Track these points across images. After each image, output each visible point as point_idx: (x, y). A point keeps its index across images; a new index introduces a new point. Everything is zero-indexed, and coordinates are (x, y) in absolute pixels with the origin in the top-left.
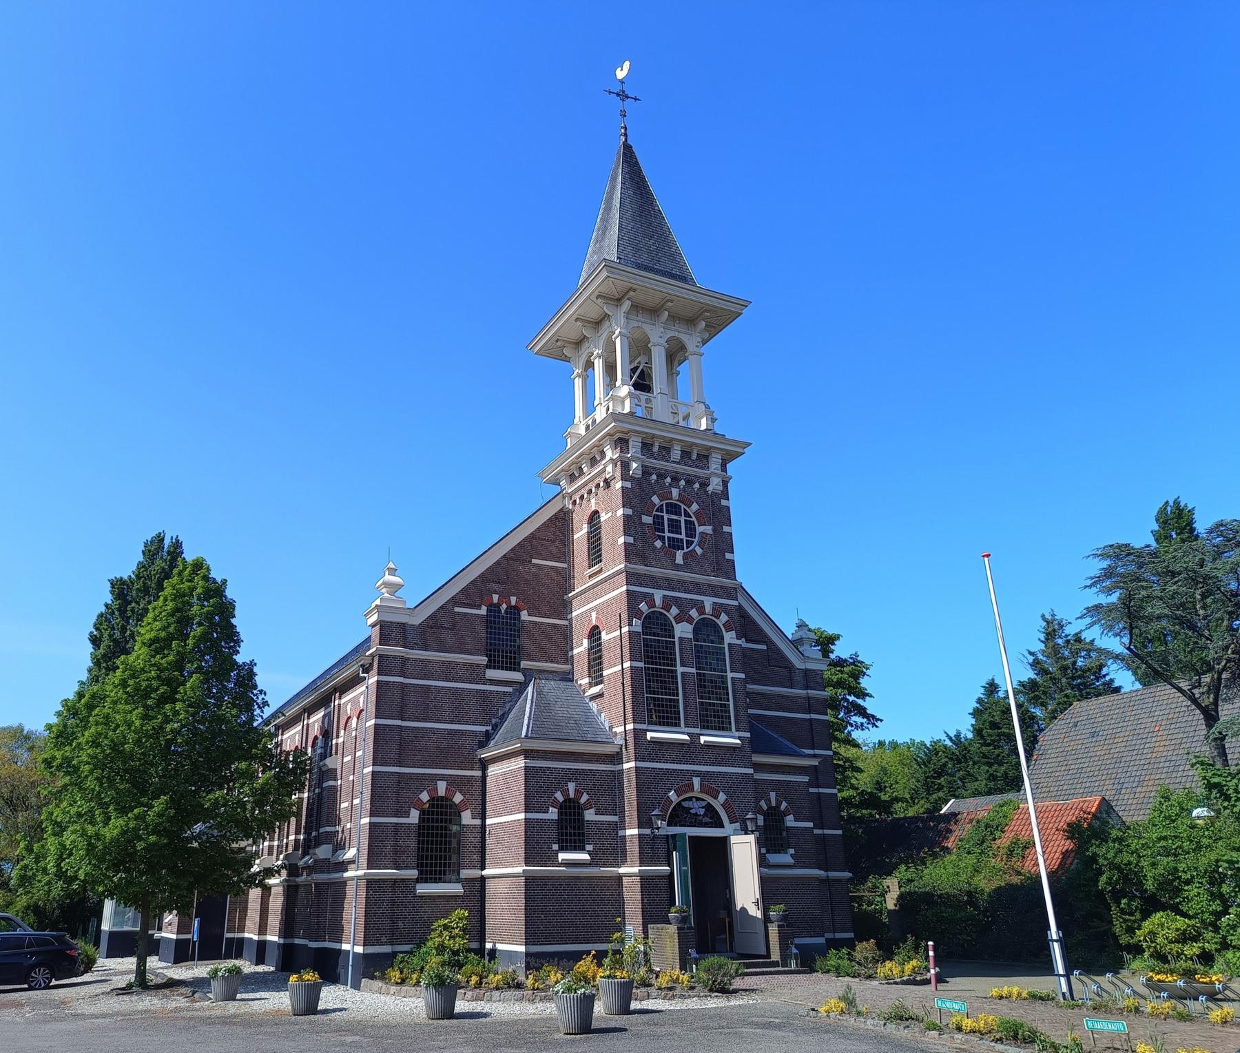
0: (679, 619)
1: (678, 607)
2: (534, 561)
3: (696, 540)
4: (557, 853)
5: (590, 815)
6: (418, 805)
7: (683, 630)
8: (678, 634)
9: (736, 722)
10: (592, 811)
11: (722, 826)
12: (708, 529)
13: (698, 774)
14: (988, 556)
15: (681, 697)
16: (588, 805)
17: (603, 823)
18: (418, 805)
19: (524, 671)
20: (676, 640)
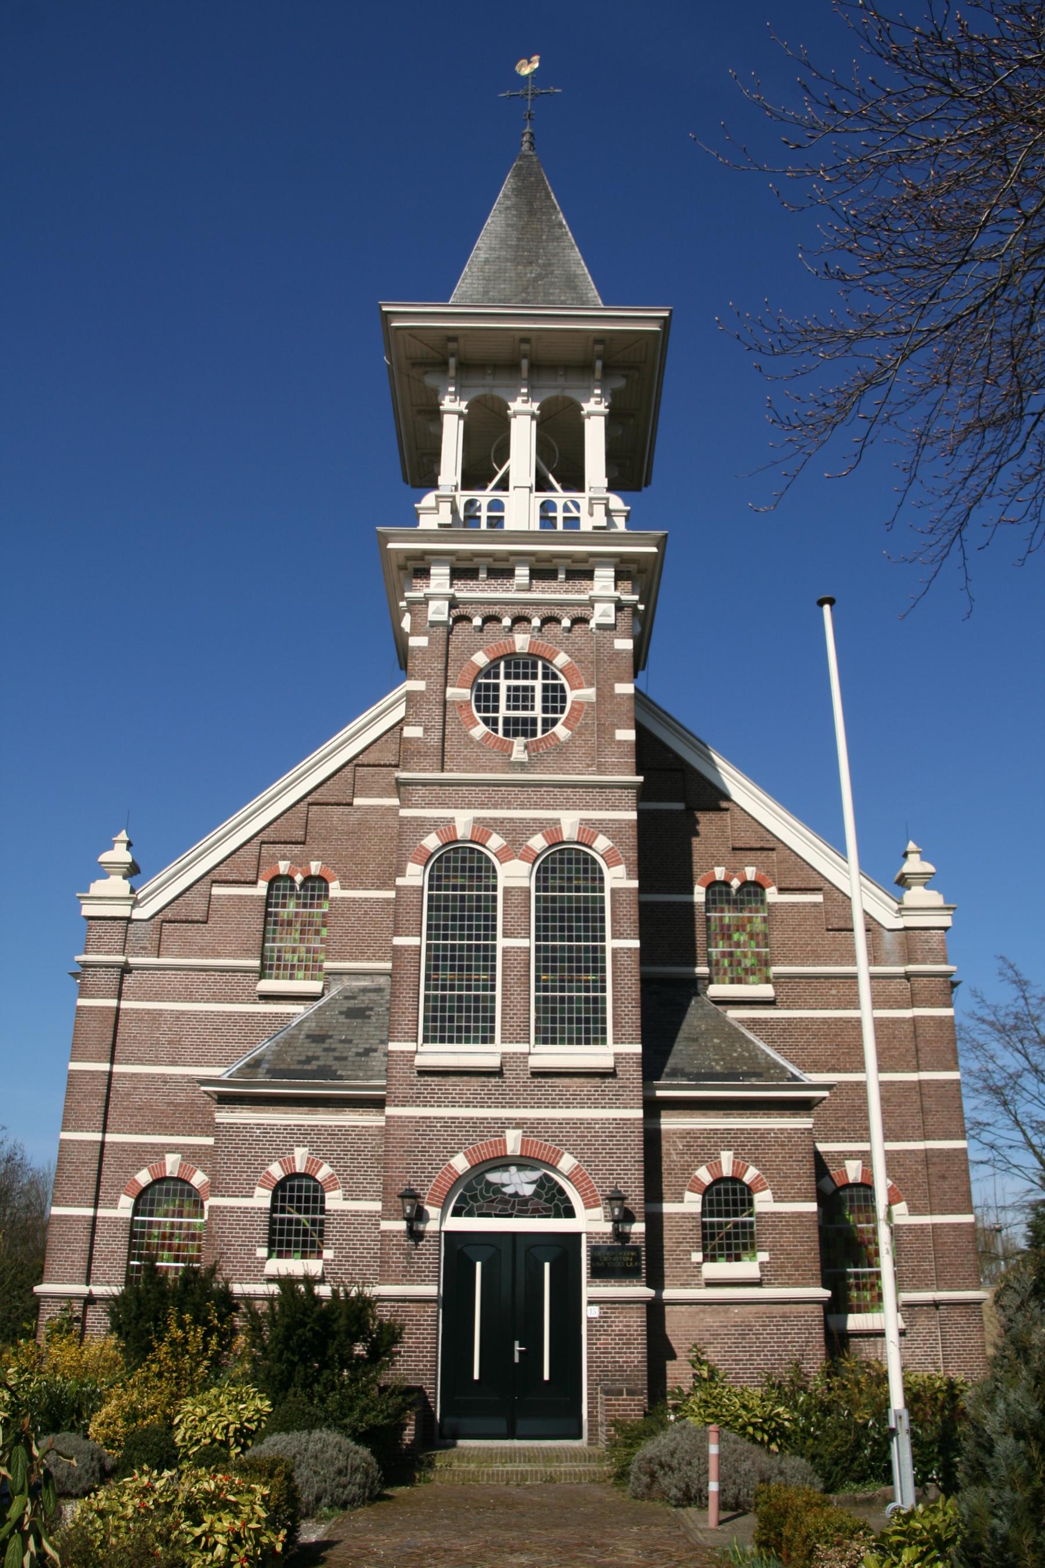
0: (504, 855)
1: (504, 836)
2: (357, 801)
3: (563, 717)
4: (263, 1261)
5: (334, 1201)
6: (695, 1185)
7: (514, 874)
8: (608, 885)
9: (615, 1026)
10: (338, 1193)
11: (570, 1213)
12: (589, 693)
13: (519, 1124)
14: (831, 602)
15: (533, 993)
16: (332, 1183)
17: (356, 1214)
18: (695, 1185)
19: (777, 981)
20: (500, 894)
